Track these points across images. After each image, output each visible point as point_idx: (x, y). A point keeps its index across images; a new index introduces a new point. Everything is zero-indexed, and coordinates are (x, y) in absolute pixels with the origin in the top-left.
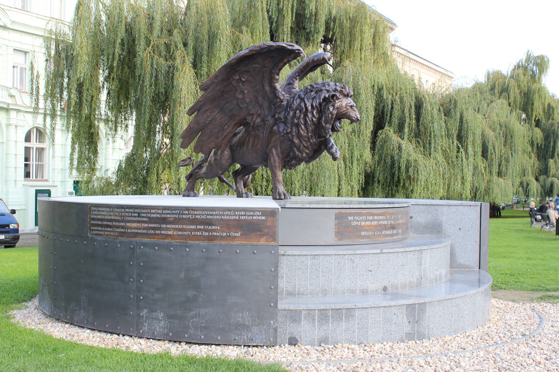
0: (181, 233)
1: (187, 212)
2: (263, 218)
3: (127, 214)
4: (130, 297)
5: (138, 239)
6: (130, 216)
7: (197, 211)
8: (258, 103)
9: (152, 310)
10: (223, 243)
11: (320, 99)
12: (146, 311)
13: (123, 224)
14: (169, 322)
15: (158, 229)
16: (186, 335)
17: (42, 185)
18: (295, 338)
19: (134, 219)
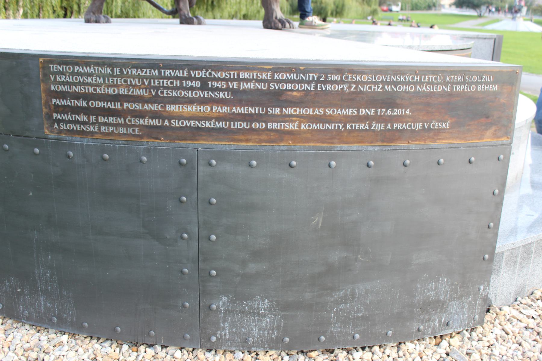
0: (318, 126)
1: (337, 78)
2: (495, 88)
4: (182, 272)
5: (201, 144)
6: (176, 88)
7: (361, 73)
9: (239, 297)
10: (414, 145)
12: (225, 298)
13: (155, 107)
14: (284, 317)
15: (257, 118)
16: (323, 338)
19: (189, 94)
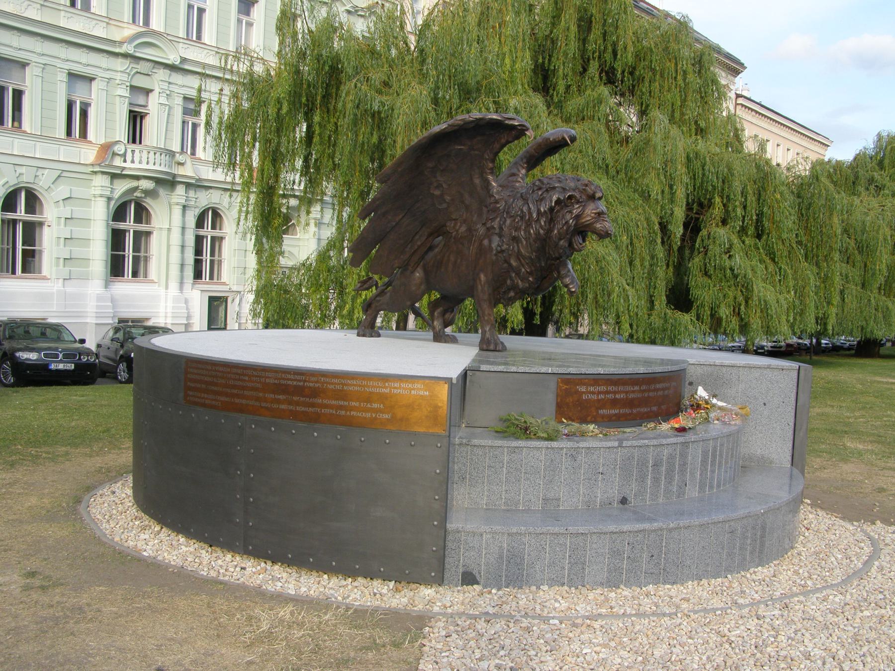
3: (233, 376)
8: (463, 202)
11: (551, 201)
17: (216, 289)
18: (471, 574)
